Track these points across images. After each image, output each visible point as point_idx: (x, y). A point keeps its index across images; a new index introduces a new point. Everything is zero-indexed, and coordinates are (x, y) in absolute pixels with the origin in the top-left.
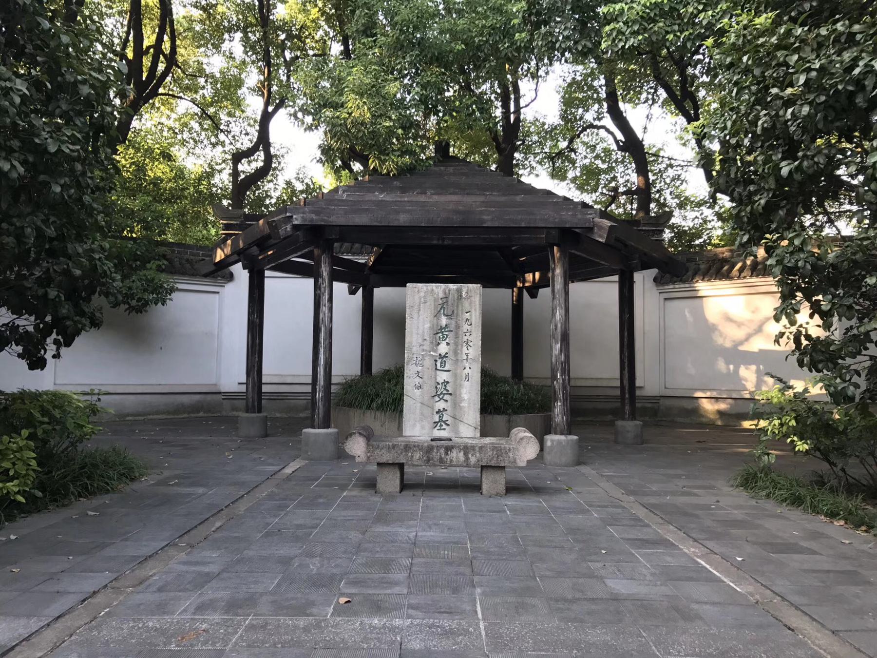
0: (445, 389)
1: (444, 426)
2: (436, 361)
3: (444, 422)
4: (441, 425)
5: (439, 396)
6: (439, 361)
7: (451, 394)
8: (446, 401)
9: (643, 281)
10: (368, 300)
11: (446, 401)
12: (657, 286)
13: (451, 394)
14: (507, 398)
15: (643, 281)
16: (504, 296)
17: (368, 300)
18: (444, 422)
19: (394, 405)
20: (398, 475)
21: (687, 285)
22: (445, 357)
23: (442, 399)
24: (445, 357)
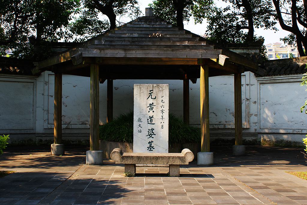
0: (152, 132)
1: (152, 149)
2: (148, 119)
3: (152, 147)
4: (151, 149)
5: (149, 135)
6: (149, 119)
7: (155, 135)
8: (153, 138)
9: (248, 77)
10: (110, 86)
11: (153, 138)
12: (256, 76)
13: (155, 135)
14: (182, 133)
15: (248, 77)
16: (180, 83)
17: (110, 86)
18: (152, 147)
19: (127, 138)
20: (65, 120)
21: (271, 77)
22: (152, 117)
23: (151, 137)
24: (152, 117)
